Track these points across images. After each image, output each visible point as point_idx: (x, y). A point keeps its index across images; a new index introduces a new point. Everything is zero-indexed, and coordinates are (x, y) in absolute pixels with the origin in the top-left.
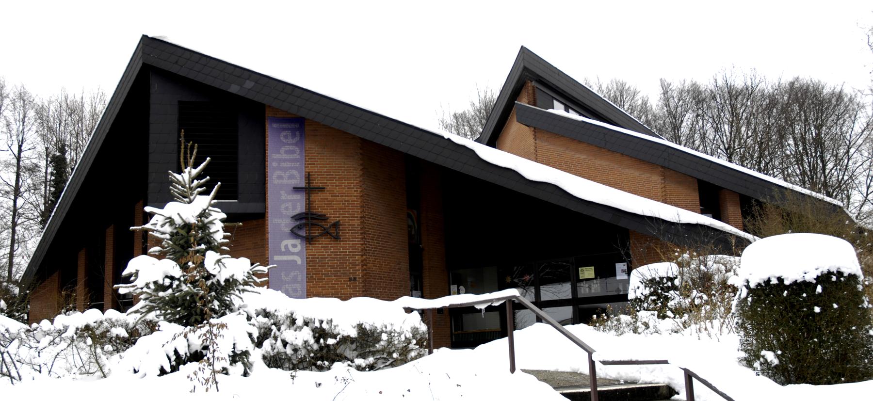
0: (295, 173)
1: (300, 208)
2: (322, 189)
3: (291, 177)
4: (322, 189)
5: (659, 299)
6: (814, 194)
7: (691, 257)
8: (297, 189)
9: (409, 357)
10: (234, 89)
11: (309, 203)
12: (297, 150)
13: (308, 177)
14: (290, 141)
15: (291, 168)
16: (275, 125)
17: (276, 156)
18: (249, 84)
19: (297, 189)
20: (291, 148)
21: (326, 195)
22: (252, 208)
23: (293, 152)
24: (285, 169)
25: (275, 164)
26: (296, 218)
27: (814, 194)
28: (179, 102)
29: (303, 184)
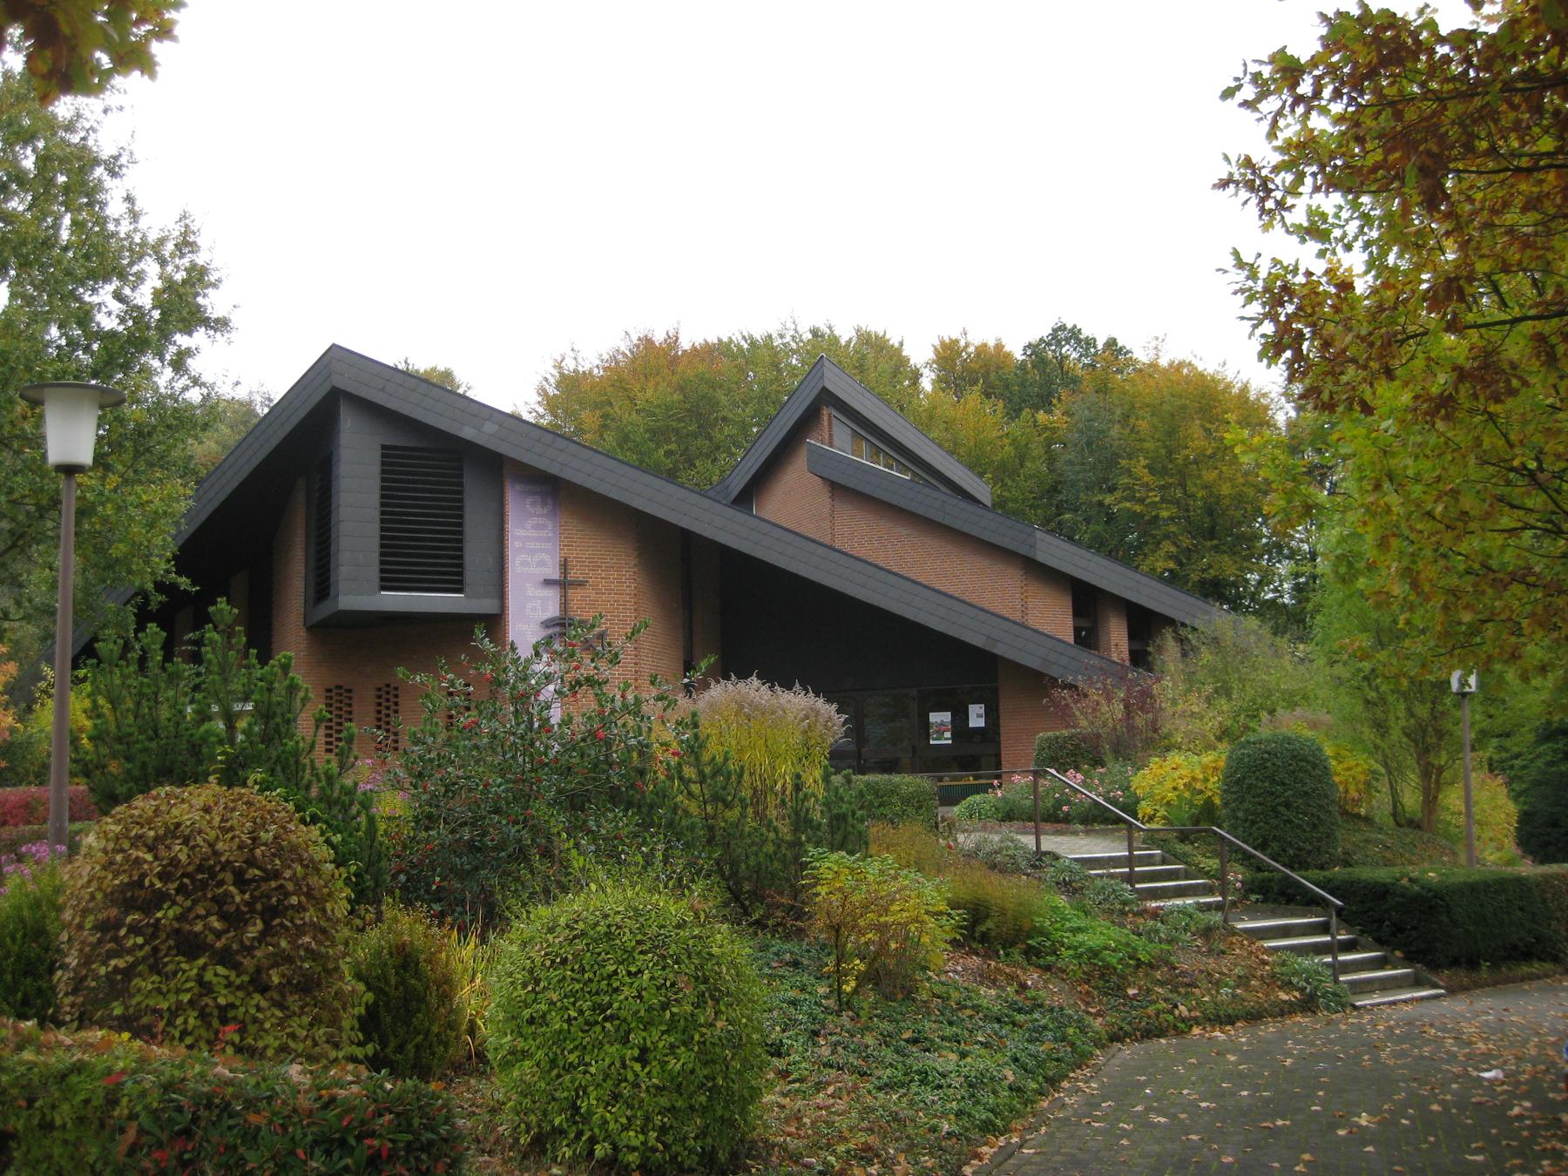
0: (545, 557)
1: (553, 611)
2: (581, 584)
3: (542, 564)
4: (581, 584)
5: (1270, 554)
6: (1050, 734)
7: (1278, 549)
8: (548, 583)
9: (1153, 1161)
10: (468, 433)
11: (565, 605)
12: (550, 524)
13: (565, 566)
14: (539, 510)
15: (541, 551)
16: (518, 487)
17: (520, 532)
18: (490, 428)
19: (548, 583)
20: (541, 521)
21: (589, 592)
22: (486, 606)
23: (544, 527)
24: (533, 552)
25: (517, 544)
26: (547, 624)
27: (1050, 734)
28: (384, 447)
29: (556, 576)
